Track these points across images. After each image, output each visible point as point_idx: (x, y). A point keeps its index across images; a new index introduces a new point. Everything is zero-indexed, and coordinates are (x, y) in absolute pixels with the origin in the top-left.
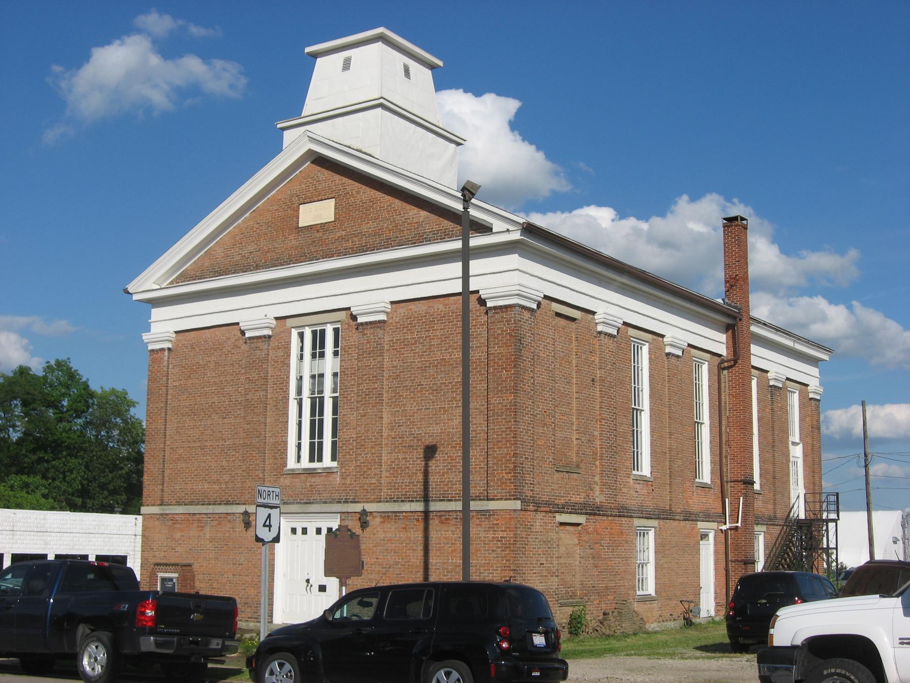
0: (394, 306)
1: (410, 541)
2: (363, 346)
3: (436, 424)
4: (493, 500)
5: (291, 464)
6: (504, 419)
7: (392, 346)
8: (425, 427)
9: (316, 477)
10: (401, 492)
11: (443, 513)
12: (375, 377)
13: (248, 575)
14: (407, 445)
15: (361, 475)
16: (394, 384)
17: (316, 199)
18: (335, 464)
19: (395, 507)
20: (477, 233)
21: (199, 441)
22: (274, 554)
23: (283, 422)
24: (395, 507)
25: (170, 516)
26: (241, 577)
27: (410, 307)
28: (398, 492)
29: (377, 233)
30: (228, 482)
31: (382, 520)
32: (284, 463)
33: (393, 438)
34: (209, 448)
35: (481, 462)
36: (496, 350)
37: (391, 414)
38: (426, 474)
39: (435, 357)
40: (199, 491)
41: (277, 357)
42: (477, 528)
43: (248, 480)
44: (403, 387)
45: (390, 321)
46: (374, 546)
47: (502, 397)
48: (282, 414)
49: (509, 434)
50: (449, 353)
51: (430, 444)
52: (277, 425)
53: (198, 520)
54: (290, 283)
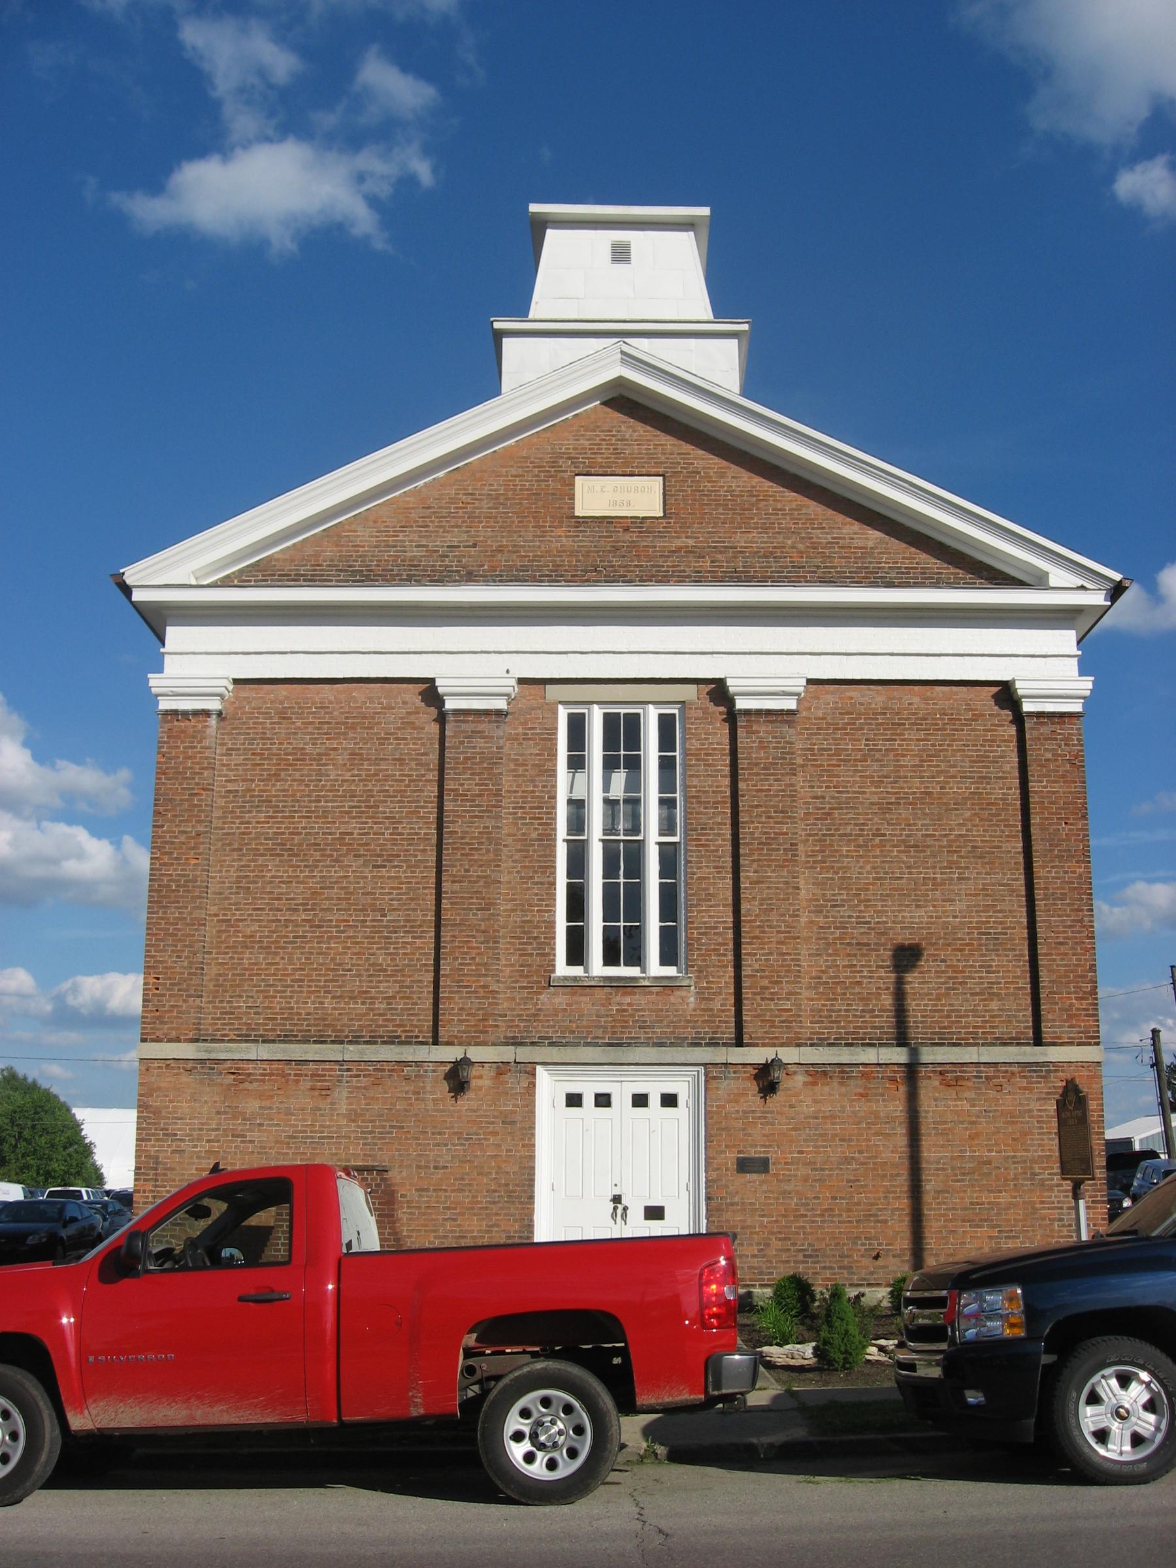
0: (812, 688)
1: (876, 1118)
2: (750, 753)
3: (917, 906)
4: (1054, 1044)
5: (562, 969)
6: (1068, 904)
7: (810, 760)
8: (893, 911)
9: (635, 994)
10: (843, 1028)
11: (948, 1068)
12: (782, 812)
13: (462, 1190)
14: (855, 941)
15: (755, 994)
16: (820, 830)
17: (618, 471)
18: (671, 971)
19: (844, 1055)
20: (992, 583)
21: (305, 910)
22: (534, 1145)
23: (542, 883)
24: (844, 1055)
25: (228, 1064)
26: (442, 1194)
27: (848, 694)
28: (838, 1028)
29: (771, 553)
30: (394, 997)
31: (810, 1079)
32: (548, 965)
33: (822, 928)
34: (336, 926)
35: (1018, 977)
36: (1045, 787)
37: (814, 884)
38: (900, 996)
39: (909, 788)
40: (308, 1014)
41: (522, 755)
42: (1024, 1093)
43: (457, 996)
44: (840, 835)
45: (804, 714)
46: (793, 1129)
47: (1063, 867)
48: (540, 867)
49: (1080, 932)
50: (938, 782)
51: (907, 943)
52: (528, 889)
53: (312, 1075)
54: (527, 617)
